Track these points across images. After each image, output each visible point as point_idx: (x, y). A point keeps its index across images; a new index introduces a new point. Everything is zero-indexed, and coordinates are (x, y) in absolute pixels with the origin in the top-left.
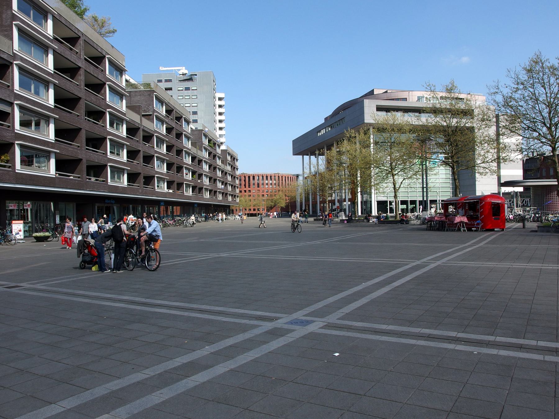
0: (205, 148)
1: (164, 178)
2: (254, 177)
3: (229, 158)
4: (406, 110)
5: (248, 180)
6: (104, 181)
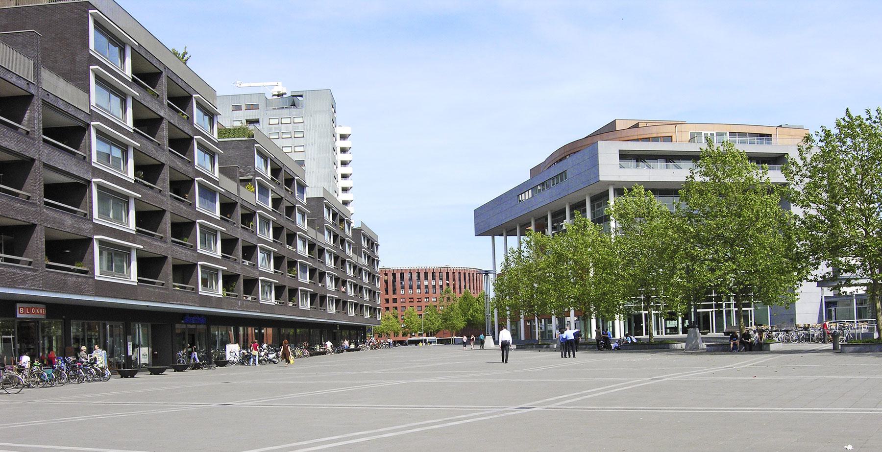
0: (328, 229)
1: (271, 283)
2: (402, 275)
3: (364, 244)
4: (670, 158)
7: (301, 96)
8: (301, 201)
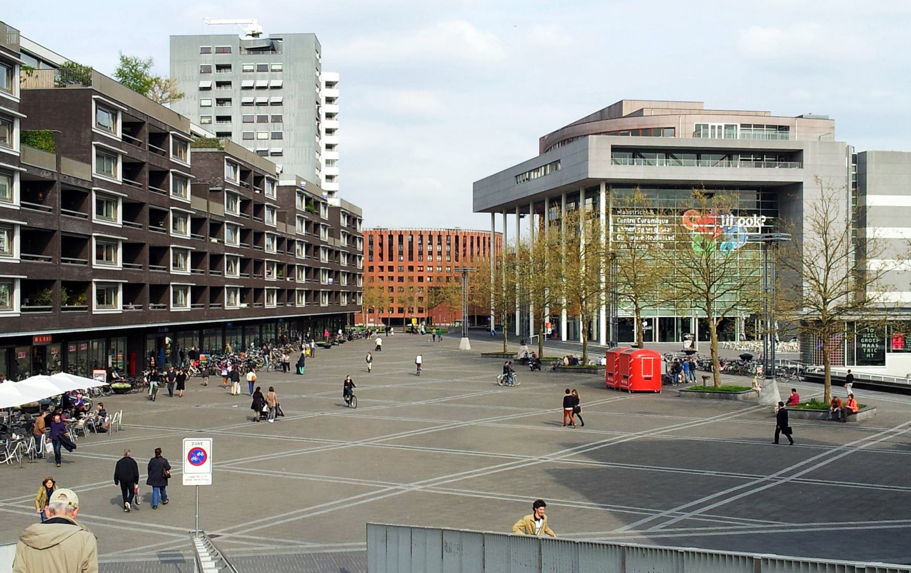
2: (401, 237)
4: (669, 153)
5: (391, 243)
6: (164, 307)
8: (270, 192)
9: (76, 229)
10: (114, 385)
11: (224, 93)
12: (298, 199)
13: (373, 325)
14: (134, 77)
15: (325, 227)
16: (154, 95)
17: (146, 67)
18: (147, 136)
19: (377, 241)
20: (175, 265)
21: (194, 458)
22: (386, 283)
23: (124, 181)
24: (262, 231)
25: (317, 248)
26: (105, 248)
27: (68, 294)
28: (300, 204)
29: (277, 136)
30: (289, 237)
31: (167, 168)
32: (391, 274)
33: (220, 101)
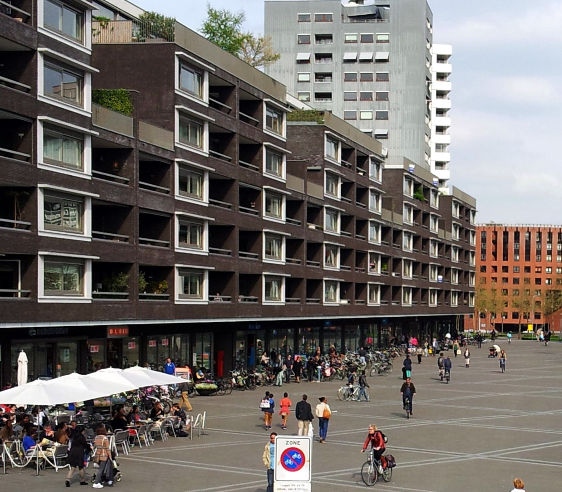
2: (517, 234)
5: (505, 240)
6: (255, 300)
7: (388, 6)
8: (375, 175)
9: (155, 204)
10: (198, 386)
11: (324, 66)
12: (405, 183)
13: (484, 331)
14: (222, 31)
15: (435, 218)
16: (247, 57)
17: (237, 21)
18: (237, 102)
19: (490, 237)
20: (268, 253)
21: (290, 462)
22: (499, 285)
23: (211, 154)
24: (365, 218)
25: (426, 241)
26: (189, 230)
27: (147, 280)
28: (408, 191)
29: (382, 116)
30: (394, 226)
31: (259, 140)
32: (505, 275)
33: (320, 76)
